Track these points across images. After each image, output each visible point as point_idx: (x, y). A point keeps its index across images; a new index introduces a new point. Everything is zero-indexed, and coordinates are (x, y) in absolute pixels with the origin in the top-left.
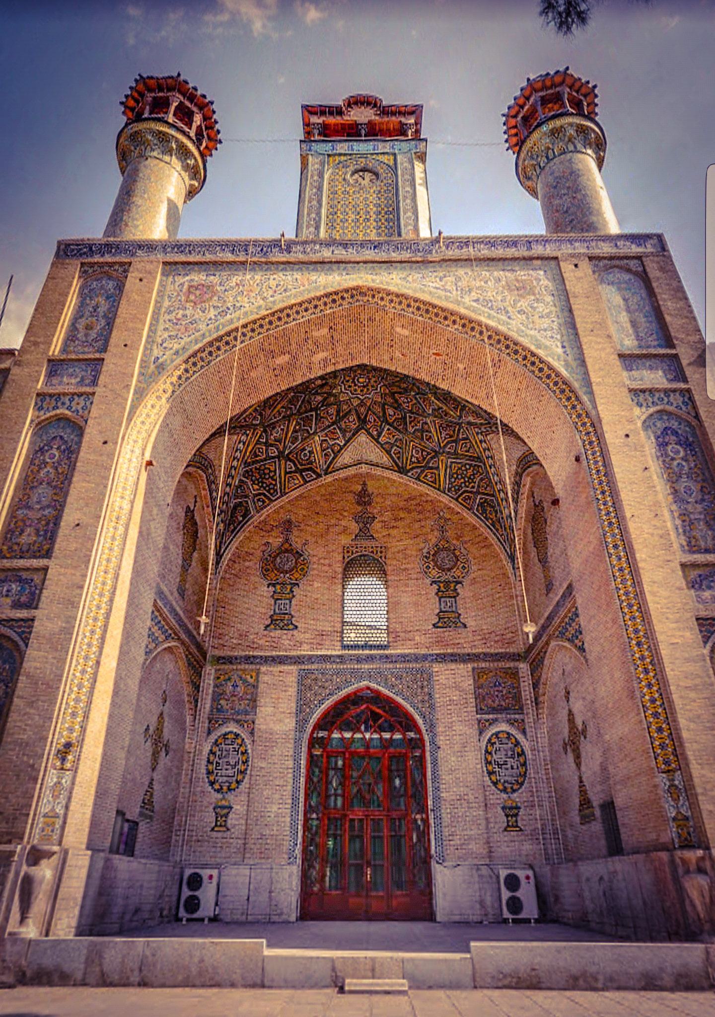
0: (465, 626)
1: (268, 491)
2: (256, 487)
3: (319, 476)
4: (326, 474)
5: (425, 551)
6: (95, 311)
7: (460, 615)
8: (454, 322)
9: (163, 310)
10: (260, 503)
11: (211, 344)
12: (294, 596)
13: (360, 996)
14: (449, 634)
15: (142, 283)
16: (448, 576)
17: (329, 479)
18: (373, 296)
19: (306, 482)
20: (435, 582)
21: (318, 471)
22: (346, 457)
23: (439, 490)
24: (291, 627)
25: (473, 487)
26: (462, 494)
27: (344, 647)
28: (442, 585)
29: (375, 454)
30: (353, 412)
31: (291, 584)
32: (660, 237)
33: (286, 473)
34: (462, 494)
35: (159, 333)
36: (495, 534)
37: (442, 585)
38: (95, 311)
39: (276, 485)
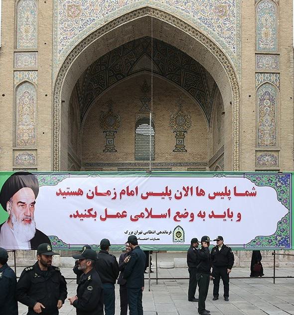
0: (186, 151)
1: (101, 86)
2: (96, 85)
3: (124, 77)
4: (127, 76)
5: (172, 116)
6: (27, 20)
7: (185, 146)
8: (189, 30)
9: (59, 21)
10: (98, 92)
11: (82, 42)
12: (115, 137)
13: (246, 277)
14: (179, 154)
15: (46, 4)
16: (181, 129)
17: (129, 78)
18: (154, 12)
19: (118, 80)
20: (175, 131)
21: (124, 74)
22: (137, 67)
23: (180, 86)
24: (114, 151)
25: (196, 86)
26: (190, 89)
27: (136, 159)
28: (178, 133)
29: (152, 66)
30: (141, 45)
31: (113, 131)
32: (179, 226)
33: (109, 77)
34: (190, 89)
35: (59, 36)
36: (203, 109)
37: (178, 133)
38: (27, 20)
39: (104, 83)
